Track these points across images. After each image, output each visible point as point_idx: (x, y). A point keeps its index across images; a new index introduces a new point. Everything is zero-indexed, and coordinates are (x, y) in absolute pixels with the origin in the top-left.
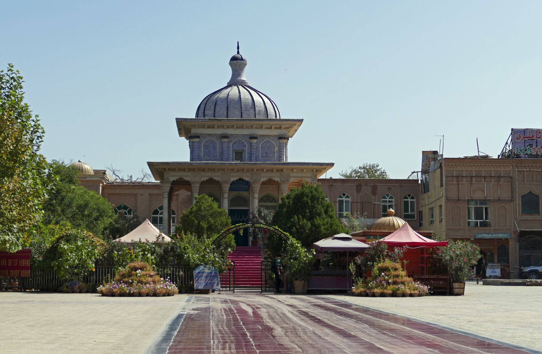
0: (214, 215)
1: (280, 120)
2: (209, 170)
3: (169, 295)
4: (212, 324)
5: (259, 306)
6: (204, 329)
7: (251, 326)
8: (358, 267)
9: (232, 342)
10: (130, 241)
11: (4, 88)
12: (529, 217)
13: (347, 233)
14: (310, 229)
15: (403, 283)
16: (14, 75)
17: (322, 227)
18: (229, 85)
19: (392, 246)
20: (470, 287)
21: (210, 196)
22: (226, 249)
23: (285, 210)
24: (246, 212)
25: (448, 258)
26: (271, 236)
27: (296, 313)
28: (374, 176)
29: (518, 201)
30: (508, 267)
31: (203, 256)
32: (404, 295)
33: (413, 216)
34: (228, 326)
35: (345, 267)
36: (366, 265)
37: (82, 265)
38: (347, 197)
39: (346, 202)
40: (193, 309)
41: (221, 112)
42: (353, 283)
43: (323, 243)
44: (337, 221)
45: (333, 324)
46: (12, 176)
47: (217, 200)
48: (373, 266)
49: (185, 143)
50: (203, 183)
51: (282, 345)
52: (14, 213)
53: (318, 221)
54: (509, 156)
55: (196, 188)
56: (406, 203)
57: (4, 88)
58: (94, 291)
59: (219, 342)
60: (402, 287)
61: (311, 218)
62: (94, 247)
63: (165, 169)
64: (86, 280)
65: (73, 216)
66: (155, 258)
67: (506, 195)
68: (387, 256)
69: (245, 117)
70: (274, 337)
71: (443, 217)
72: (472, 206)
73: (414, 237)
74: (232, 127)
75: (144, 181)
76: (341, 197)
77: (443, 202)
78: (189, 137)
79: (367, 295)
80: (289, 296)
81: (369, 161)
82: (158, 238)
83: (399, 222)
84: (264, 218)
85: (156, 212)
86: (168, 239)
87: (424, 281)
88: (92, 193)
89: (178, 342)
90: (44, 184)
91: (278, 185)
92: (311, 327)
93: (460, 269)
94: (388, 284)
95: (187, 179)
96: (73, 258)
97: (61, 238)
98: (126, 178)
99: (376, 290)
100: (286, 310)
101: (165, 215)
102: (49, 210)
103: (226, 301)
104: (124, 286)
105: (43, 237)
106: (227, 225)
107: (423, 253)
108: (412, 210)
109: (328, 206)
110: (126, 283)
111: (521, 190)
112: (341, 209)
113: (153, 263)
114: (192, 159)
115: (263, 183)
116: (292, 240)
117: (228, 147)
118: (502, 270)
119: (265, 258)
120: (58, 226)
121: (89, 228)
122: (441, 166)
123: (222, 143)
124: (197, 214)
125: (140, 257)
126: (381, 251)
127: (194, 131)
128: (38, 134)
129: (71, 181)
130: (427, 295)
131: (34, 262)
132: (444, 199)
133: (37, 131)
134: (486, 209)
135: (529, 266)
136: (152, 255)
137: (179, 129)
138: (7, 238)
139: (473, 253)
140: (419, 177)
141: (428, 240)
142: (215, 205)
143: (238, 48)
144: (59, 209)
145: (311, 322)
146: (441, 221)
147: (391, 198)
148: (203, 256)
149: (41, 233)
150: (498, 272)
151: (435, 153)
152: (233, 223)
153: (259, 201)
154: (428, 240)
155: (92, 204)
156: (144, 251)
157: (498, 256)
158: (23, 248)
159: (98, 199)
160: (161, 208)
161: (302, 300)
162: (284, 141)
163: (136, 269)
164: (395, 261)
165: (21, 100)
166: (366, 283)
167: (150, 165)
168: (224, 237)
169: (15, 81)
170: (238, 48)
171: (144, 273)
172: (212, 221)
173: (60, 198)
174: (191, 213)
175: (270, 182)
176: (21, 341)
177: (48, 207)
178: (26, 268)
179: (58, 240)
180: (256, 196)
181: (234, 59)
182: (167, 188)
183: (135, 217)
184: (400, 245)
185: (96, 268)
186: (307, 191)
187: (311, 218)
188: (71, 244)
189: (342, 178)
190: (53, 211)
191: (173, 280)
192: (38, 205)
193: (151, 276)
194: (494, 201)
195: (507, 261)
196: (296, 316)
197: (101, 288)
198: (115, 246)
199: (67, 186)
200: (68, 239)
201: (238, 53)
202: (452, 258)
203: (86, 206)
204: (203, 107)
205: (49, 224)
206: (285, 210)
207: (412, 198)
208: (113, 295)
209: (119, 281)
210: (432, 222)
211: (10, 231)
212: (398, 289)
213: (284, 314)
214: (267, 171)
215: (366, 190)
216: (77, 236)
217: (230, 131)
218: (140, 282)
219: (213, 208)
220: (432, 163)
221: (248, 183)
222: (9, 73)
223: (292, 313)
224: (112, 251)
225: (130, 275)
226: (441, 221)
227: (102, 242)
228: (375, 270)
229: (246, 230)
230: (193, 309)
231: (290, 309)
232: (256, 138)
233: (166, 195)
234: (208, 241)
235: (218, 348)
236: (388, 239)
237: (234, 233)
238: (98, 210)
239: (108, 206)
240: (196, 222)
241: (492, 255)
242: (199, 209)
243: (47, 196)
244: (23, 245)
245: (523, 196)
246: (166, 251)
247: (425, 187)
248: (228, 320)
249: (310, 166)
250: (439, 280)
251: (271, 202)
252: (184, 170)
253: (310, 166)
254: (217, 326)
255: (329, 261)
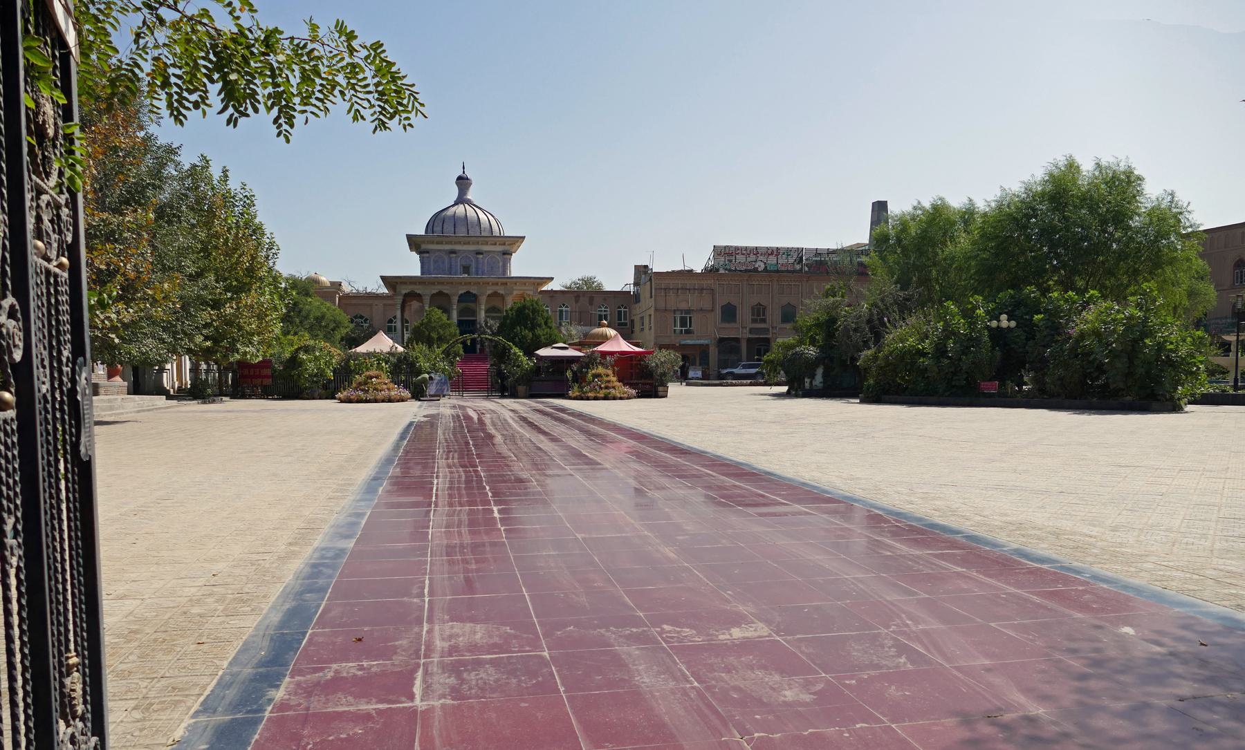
0: (444, 326)
1: (504, 237)
2: (439, 283)
3: (403, 401)
4: (440, 431)
5: (484, 412)
6: (432, 439)
7: (474, 434)
8: (574, 373)
9: (456, 452)
10: (365, 351)
11: (238, 206)
12: (727, 325)
13: (565, 343)
14: (532, 339)
15: (614, 388)
16: (247, 194)
17: (543, 337)
18: (456, 203)
19: (604, 354)
20: (674, 389)
21: (439, 308)
22: (455, 358)
23: (508, 321)
24: (474, 322)
25: (654, 364)
26: (495, 347)
27: (517, 419)
28: (591, 287)
29: (718, 311)
30: (709, 369)
31: (434, 365)
32: (614, 398)
33: (626, 324)
34: (455, 434)
35: (563, 373)
36: (582, 372)
37: (321, 373)
38: (567, 307)
39: (566, 311)
40: (424, 416)
41: (449, 229)
42: (569, 388)
43: (543, 352)
44: (556, 331)
45: (547, 430)
46: (249, 290)
47: (446, 310)
48: (587, 372)
49: (415, 258)
50: (433, 295)
51: (500, 454)
52: (253, 326)
53: (539, 332)
54: (711, 271)
55: (427, 300)
56: (620, 313)
57: (238, 206)
58: (334, 398)
59: (444, 451)
60: (613, 391)
61: (532, 329)
62: (332, 357)
63: (397, 283)
64: (325, 387)
65: (311, 327)
66: (389, 367)
67: (708, 306)
68: (601, 363)
69: (471, 234)
70: (493, 445)
71: (652, 325)
72: (678, 316)
73: (624, 346)
74: (460, 243)
75: (378, 292)
76: (561, 307)
77: (652, 312)
78: (420, 252)
79: (582, 399)
80: (513, 400)
81: (587, 274)
82: (391, 348)
83: (611, 332)
84: (490, 328)
85: (391, 321)
86: (400, 349)
87: (632, 386)
88: (328, 304)
89: (406, 452)
90: (281, 298)
91: (502, 297)
92: (527, 433)
93: (664, 374)
94: (601, 388)
95: (418, 292)
96: (311, 368)
97: (299, 349)
98: (361, 289)
99: (590, 394)
100: (508, 415)
101: (399, 325)
102: (288, 321)
103: (454, 407)
104: (360, 393)
105: (282, 348)
106: (455, 335)
107: (632, 360)
108: (625, 319)
109: (547, 318)
110: (362, 390)
111: (722, 301)
112: (561, 318)
113: (387, 372)
114: (422, 273)
115: (489, 296)
116: (515, 350)
117: (456, 262)
118: (703, 372)
119: (491, 365)
120: (296, 337)
121: (327, 338)
122: (650, 280)
123: (451, 258)
124: (428, 325)
125: (375, 366)
126: (595, 359)
127: (424, 247)
128: (273, 251)
129: (307, 295)
130: (635, 398)
131: (275, 371)
132: (653, 309)
133: (272, 248)
134: (690, 318)
135: (726, 368)
136: (386, 364)
137: (410, 245)
138: (248, 350)
139: (676, 360)
140: (632, 289)
141: (637, 349)
142: (444, 317)
143: (464, 168)
144: (297, 320)
145: (528, 428)
146: (650, 329)
147: (606, 307)
148: (434, 365)
149: (280, 344)
150: (699, 374)
151: (646, 267)
152: (461, 334)
153: (486, 312)
154: (637, 349)
155: (328, 315)
156: (378, 360)
157: (700, 359)
158: (263, 359)
159: (334, 310)
160: (395, 317)
161: (524, 404)
162: (508, 256)
163: (371, 377)
164: (607, 368)
165: (255, 217)
166: (581, 388)
167: (383, 278)
168: (453, 347)
169: (248, 199)
170: (464, 168)
171: (380, 381)
172: (442, 332)
173: (297, 310)
174: (422, 324)
175: (495, 294)
176: (261, 454)
177: (285, 319)
178: (267, 377)
179: (297, 350)
180: (483, 307)
181: (460, 178)
182: (399, 300)
183: (371, 326)
184: (612, 353)
185: (334, 376)
186: (528, 304)
187: (532, 329)
188: (310, 354)
189: (563, 289)
190: (291, 323)
191: (406, 387)
192: (275, 319)
193: (386, 384)
194: (697, 310)
195: (708, 364)
196: (516, 422)
197: (339, 395)
198: (351, 356)
199: (303, 298)
200: (307, 349)
201: (464, 172)
202: (657, 365)
203: (323, 317)
204: (431, 224)
205: (288, 334)
206: (508, 321)
207: (625, 308)
208: (350, 401)
209: (356, 389)
210: (642, 330)
211: (251, 343)
212: (610, 393)
213: (505, 420)
214: (493, 284)
215: (584, 301)
216: (315, 347)
217: (458, 247)
218: (375, 389)
219: (442, 320)
220: (643, 276)
221: (475, 296)
222: (242, 191)
223: (513, 419)
224: (349, 361)
225: (366, 383)
226: (650, 329)
227: (339, 351)
228: (589, 376)
229: (473, 341)
230: (424, 416)
231: (511, 414)
232: (482, 254)
233: (399, 307)
234: (438, 351)
235: (442, 458)
236: (600, 348)
237: (462, 343)
238: (335, 322)
239: (344, 318)
240: (427, 333)
241: (695, 358)
242: (430, 321)
243: (284, 311)
244: (264, 356)
245: (722, 307)
246: (399, 360)
247: (636, 298)
248: (454, 428)
249: (532, 280)
250: (646, 384)
251: (496, 313)
252: (414, 283)
253: (532, 280)
254: (444, 434)
255: (548, 368)
